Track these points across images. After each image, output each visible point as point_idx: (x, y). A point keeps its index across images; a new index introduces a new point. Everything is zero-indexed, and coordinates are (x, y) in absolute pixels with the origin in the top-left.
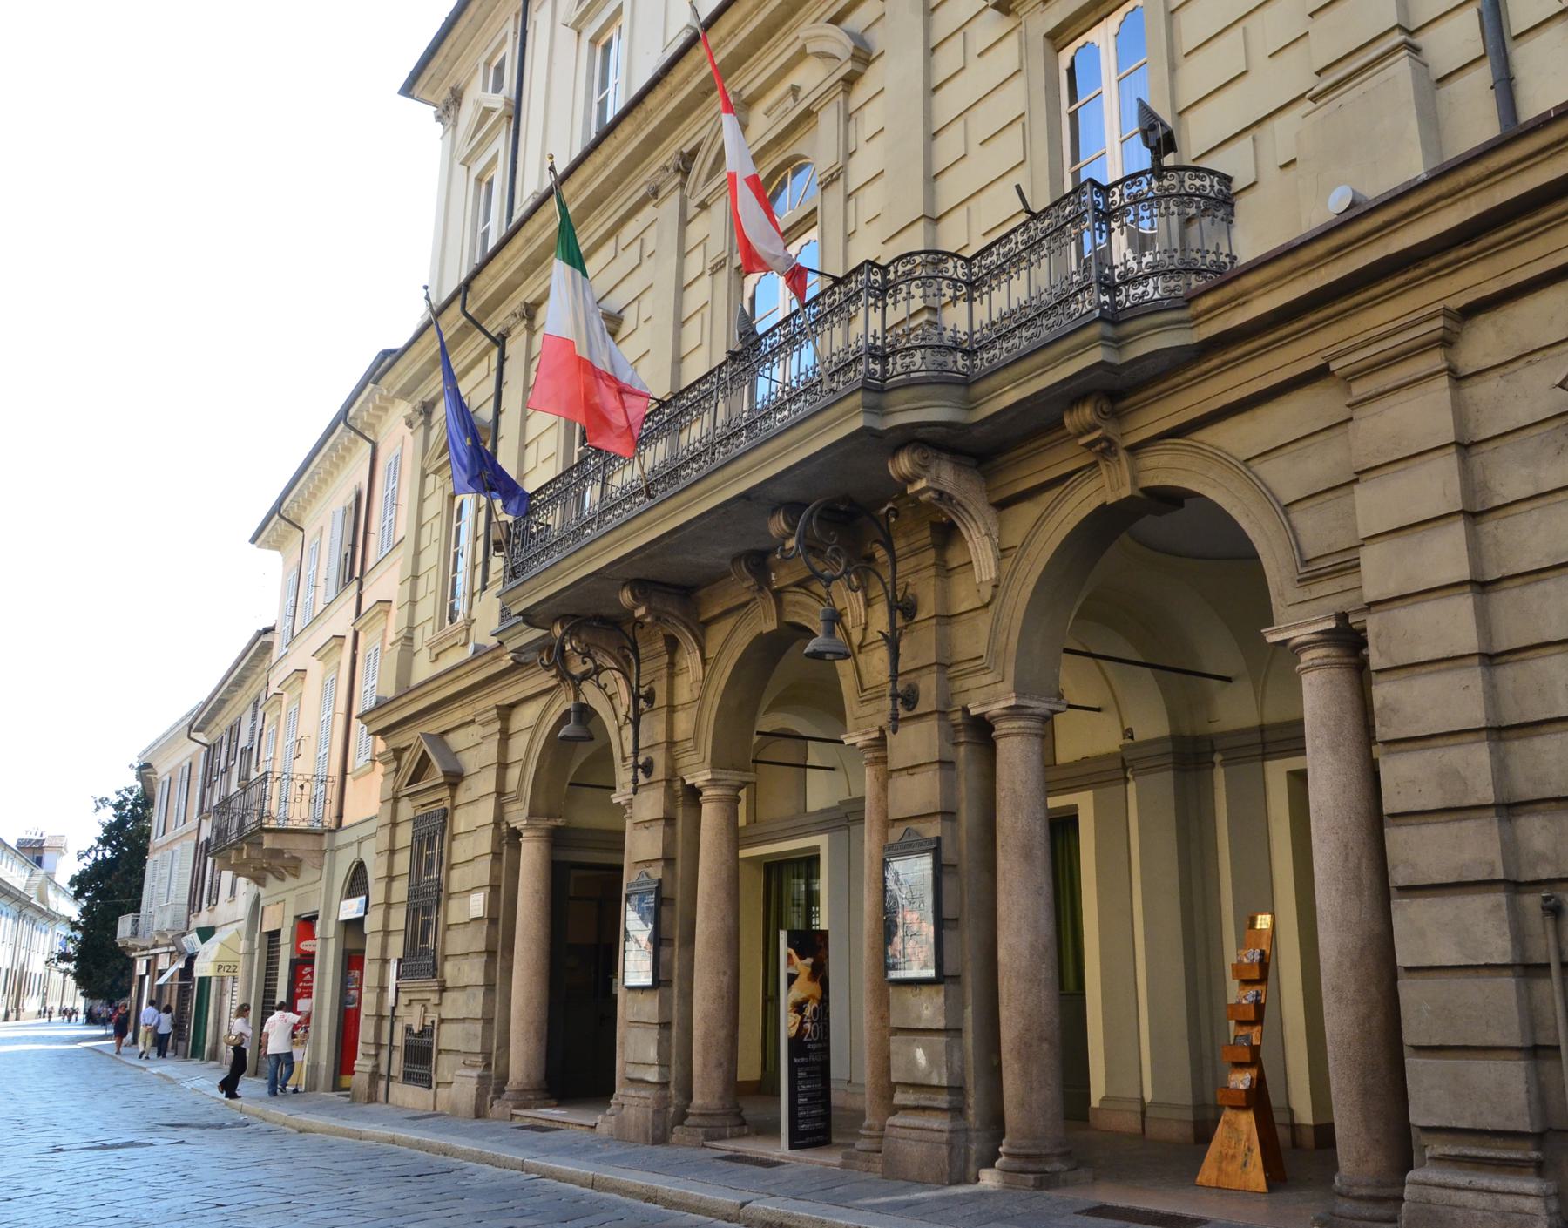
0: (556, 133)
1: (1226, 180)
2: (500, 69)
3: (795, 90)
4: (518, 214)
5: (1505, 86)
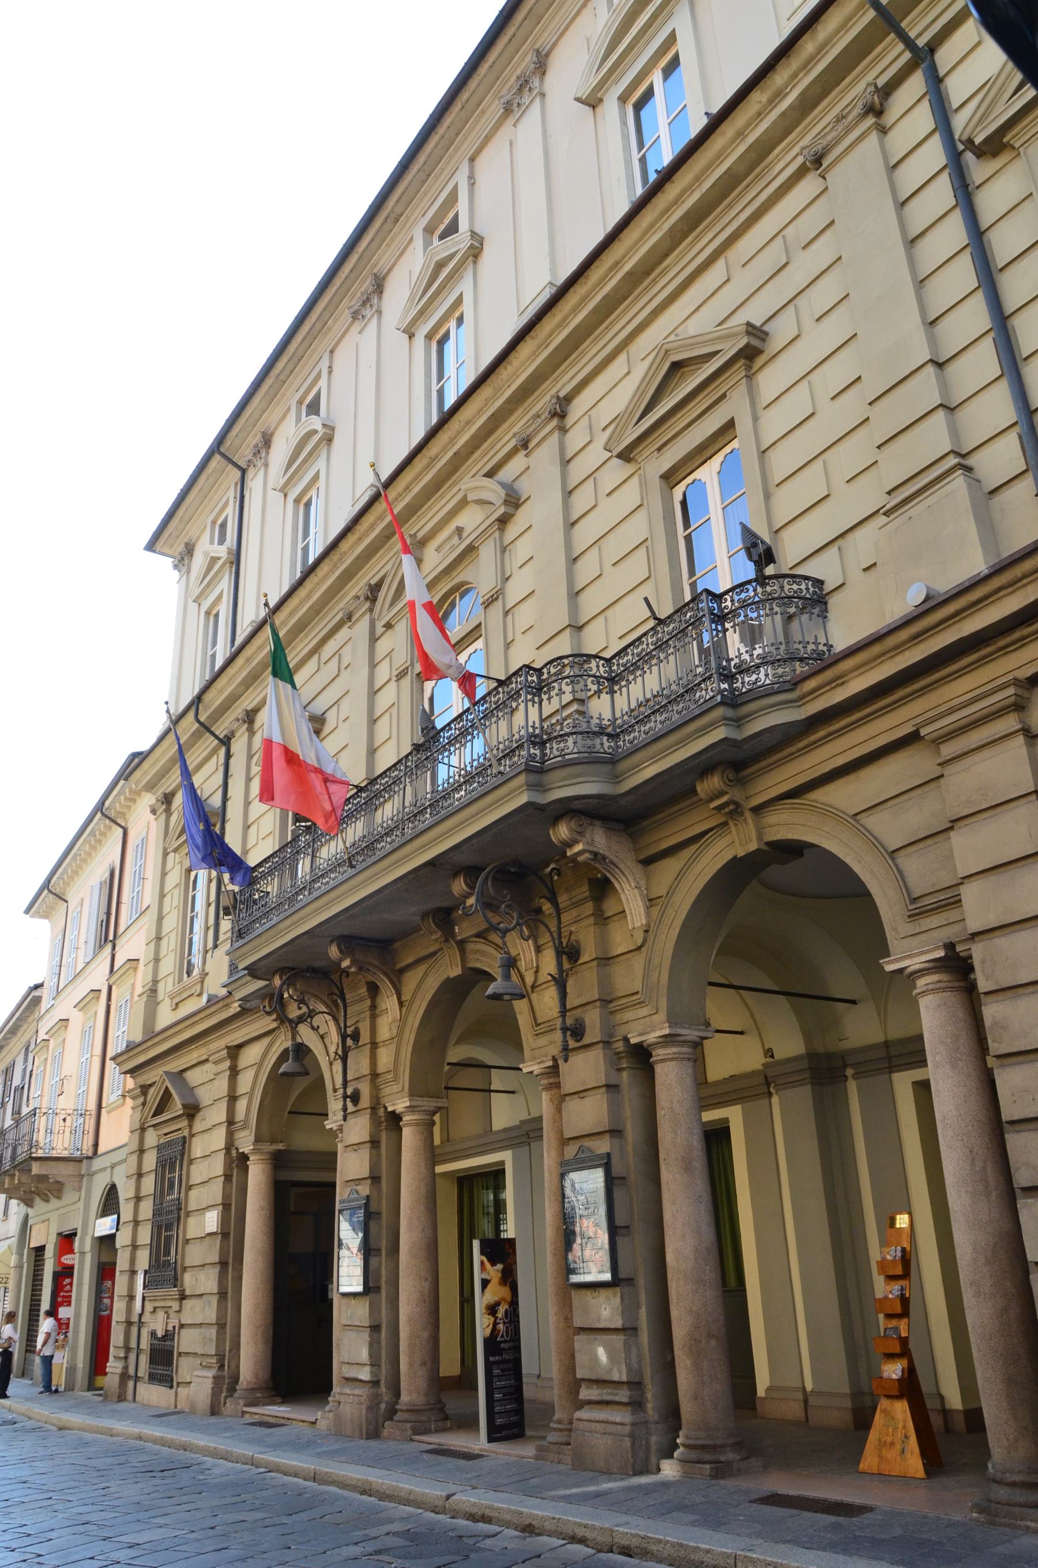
1: (819, 583)
2: (223, 526)
3: (459, 530)
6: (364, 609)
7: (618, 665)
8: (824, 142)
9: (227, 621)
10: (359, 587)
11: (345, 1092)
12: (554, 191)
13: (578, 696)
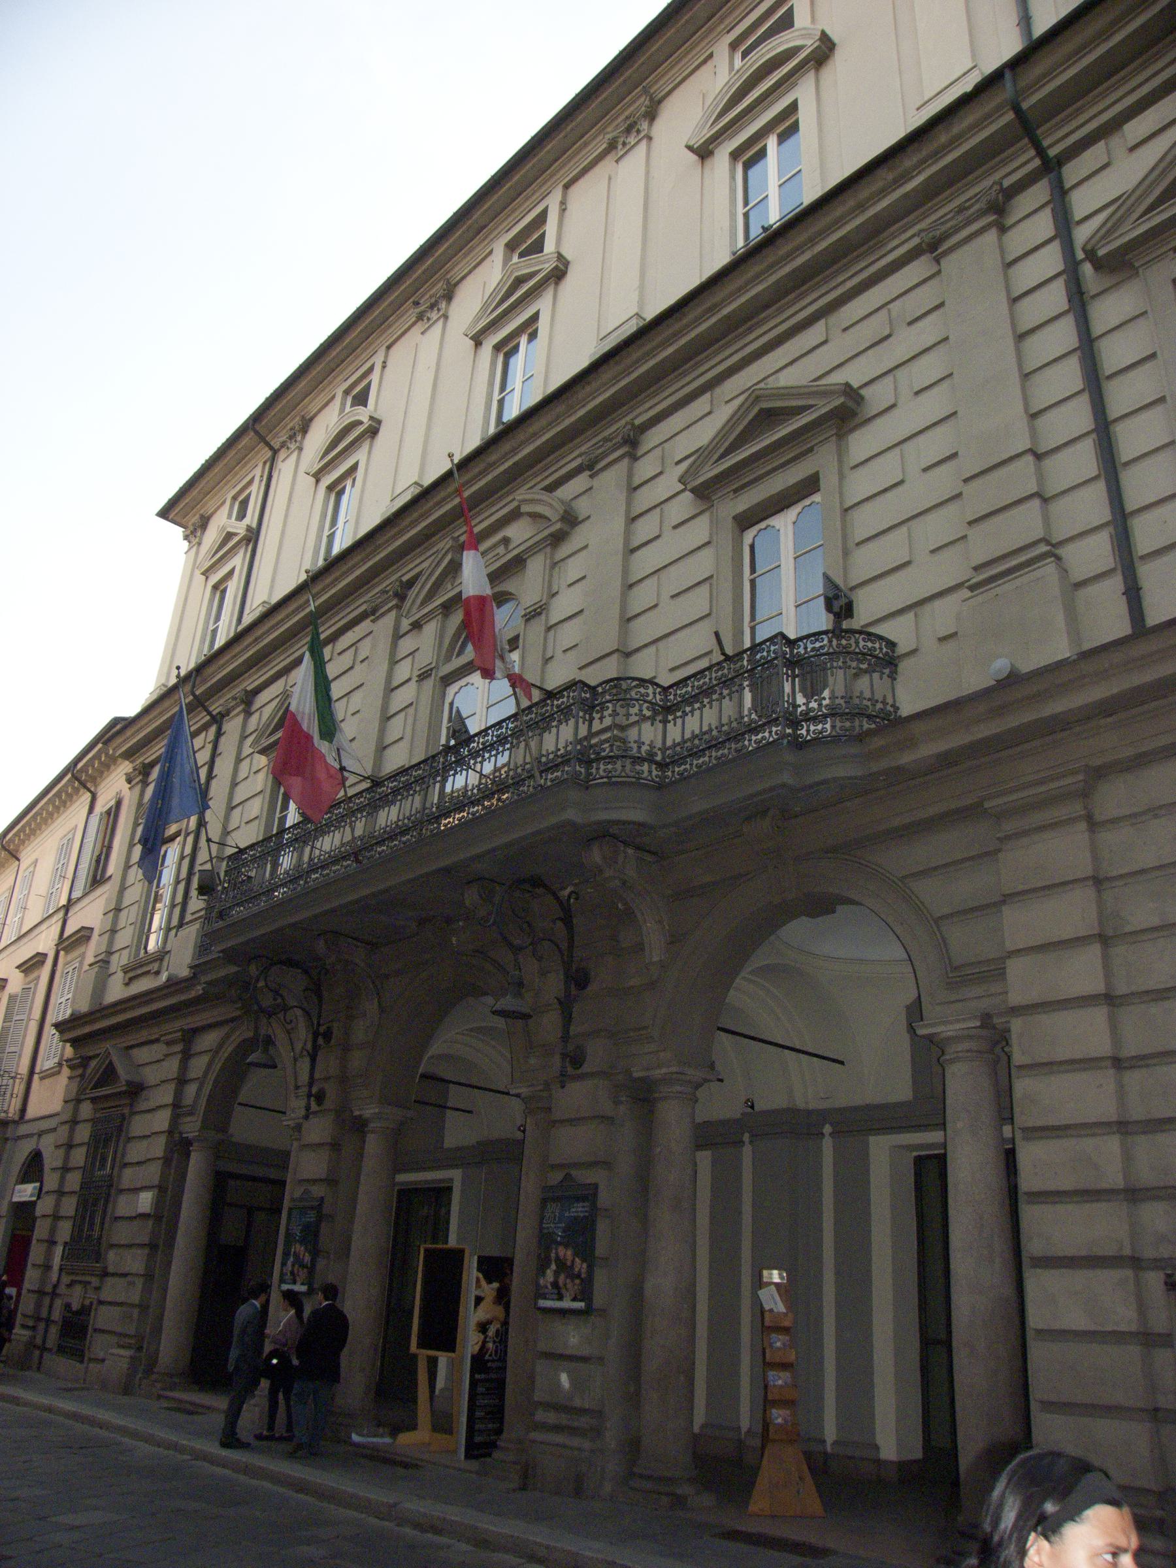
0: (282, 566)
1: (892, 645)
2: (244, 504)
3: (506, 541)
4: (247, 619)
5: (1133, 594)
6: (390, 605)
7: (675, 695)
8: (943, 228)
9: (235, 597)
10: (388, 582)
11: (310, 1091)
12: (649, 235)
13: (618, 720)
